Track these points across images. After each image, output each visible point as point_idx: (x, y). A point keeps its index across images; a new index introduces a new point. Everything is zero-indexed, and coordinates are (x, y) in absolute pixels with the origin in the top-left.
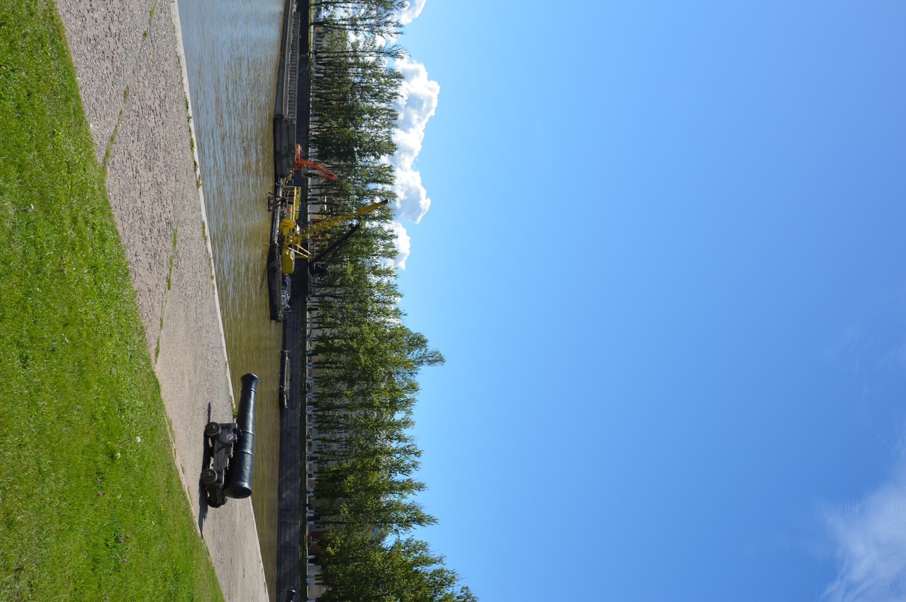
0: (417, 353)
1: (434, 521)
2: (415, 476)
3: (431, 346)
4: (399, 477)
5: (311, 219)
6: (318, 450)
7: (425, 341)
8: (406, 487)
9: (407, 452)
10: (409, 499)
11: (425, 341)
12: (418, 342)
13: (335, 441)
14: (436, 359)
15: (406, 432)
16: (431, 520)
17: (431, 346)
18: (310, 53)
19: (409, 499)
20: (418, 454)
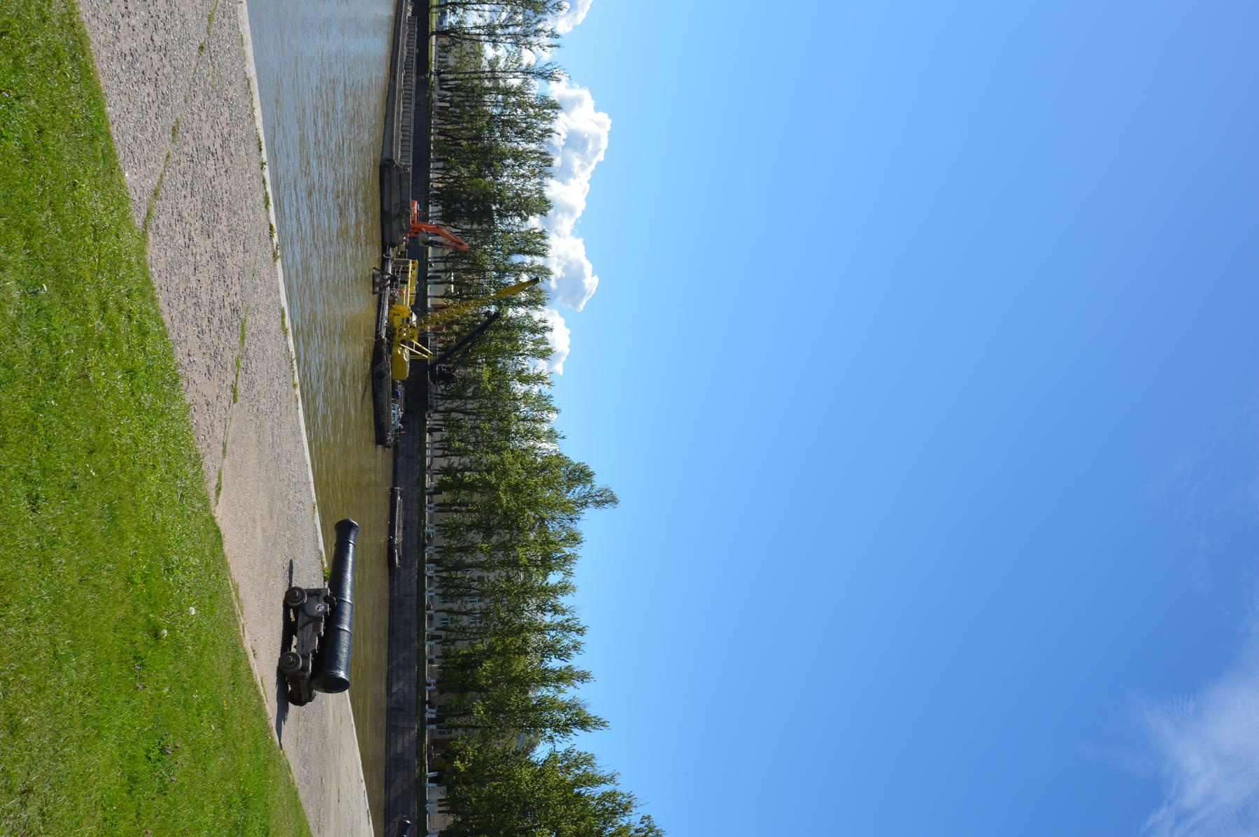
0: (579, 490)
1: (603, 724)
2: (577, 662)
3: (599, 482)
4: (554, 663)
5: (432, 305)
6: (441, 626)
7: (590, 475)
8: (564, 677)
9: (565, 628)
10: (568, 693)
11: (590, 475)
12: (581, 475)
13: (465, 613)
14: (606, 499)
15: (564, 601)
16: (599, 723)
17: (599, 482)
18: (431, 73)
19: (568, 693)
20: (580, 631)
